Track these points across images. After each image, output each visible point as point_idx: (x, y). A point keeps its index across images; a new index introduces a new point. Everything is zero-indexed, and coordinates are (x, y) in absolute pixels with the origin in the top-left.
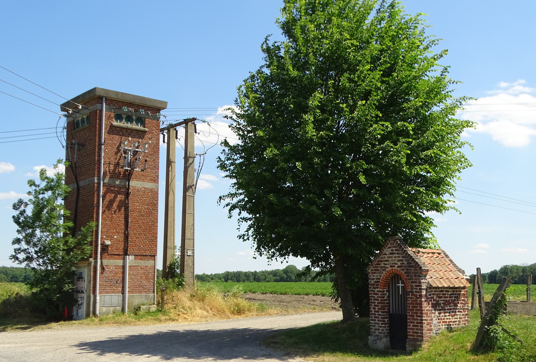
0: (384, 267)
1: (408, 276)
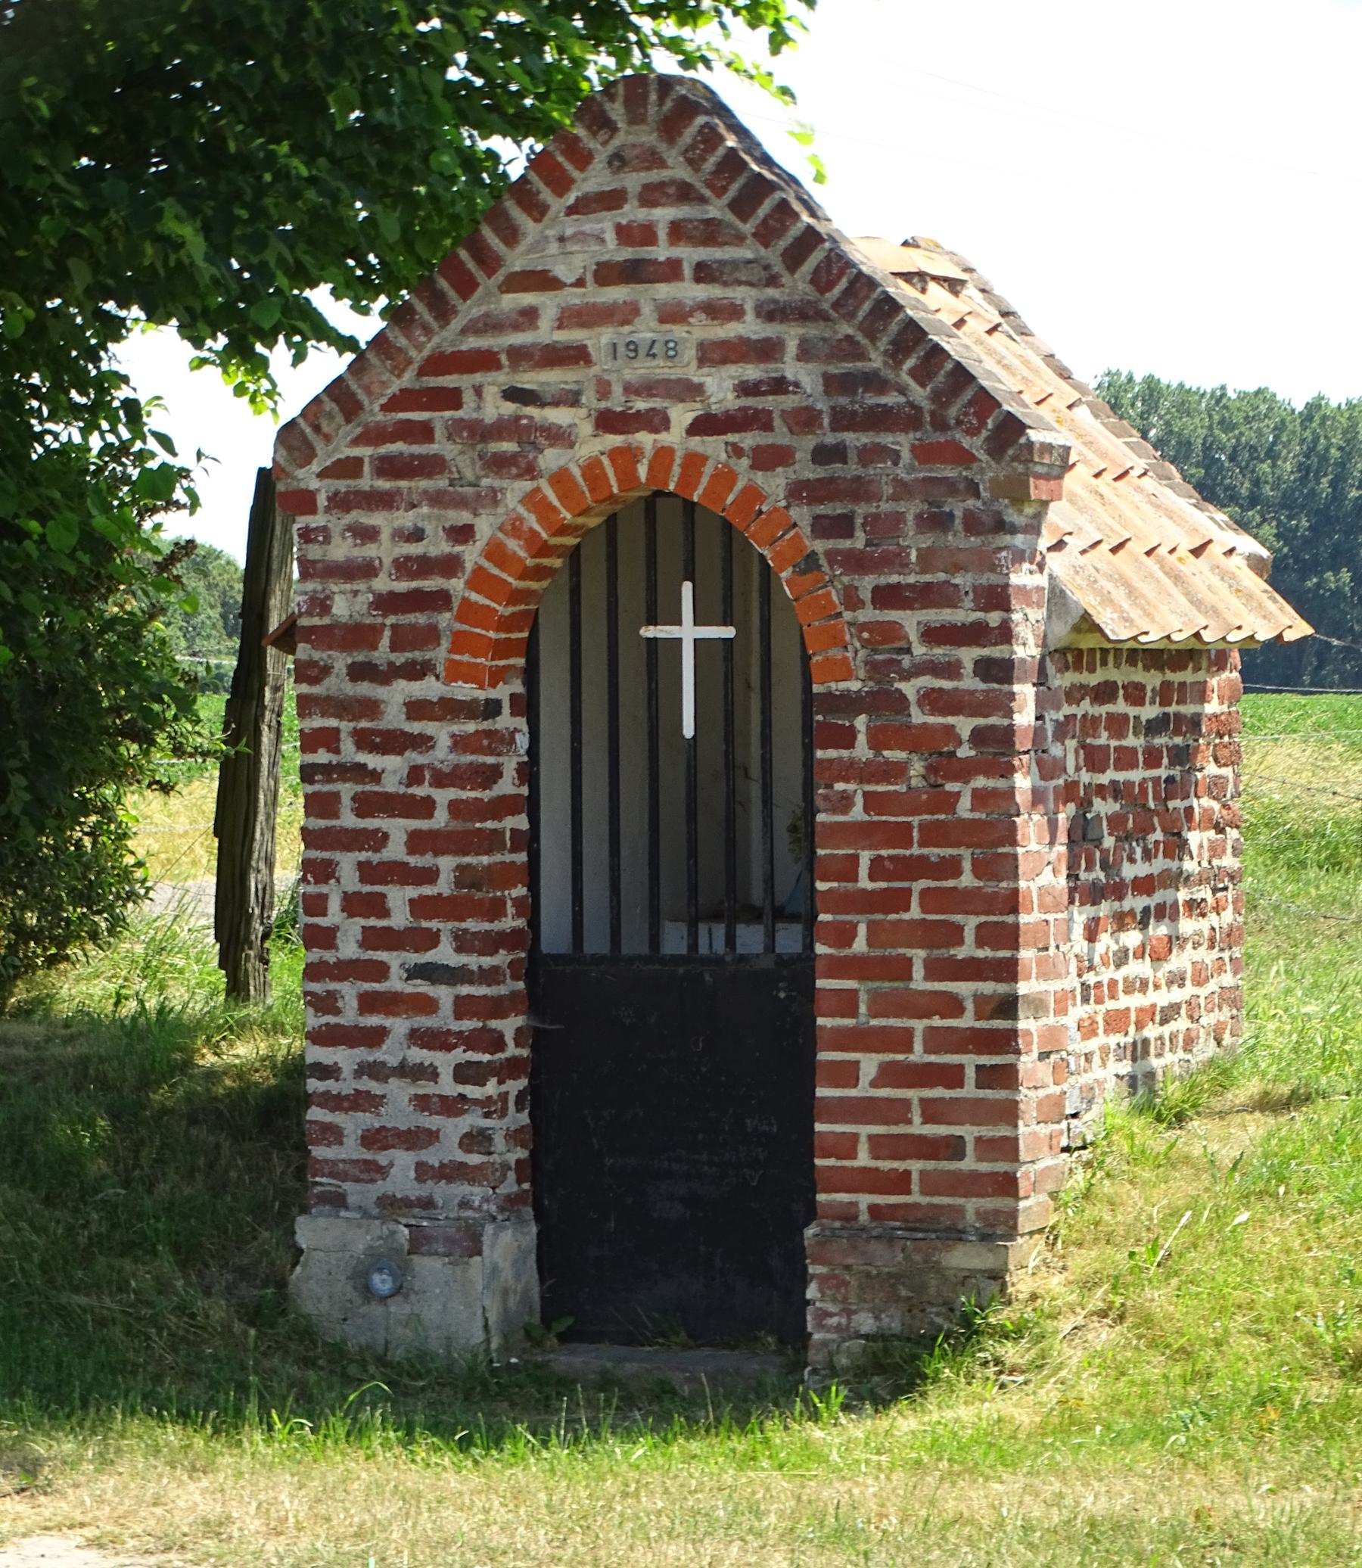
0: (502, 429)
1: (824, 527)
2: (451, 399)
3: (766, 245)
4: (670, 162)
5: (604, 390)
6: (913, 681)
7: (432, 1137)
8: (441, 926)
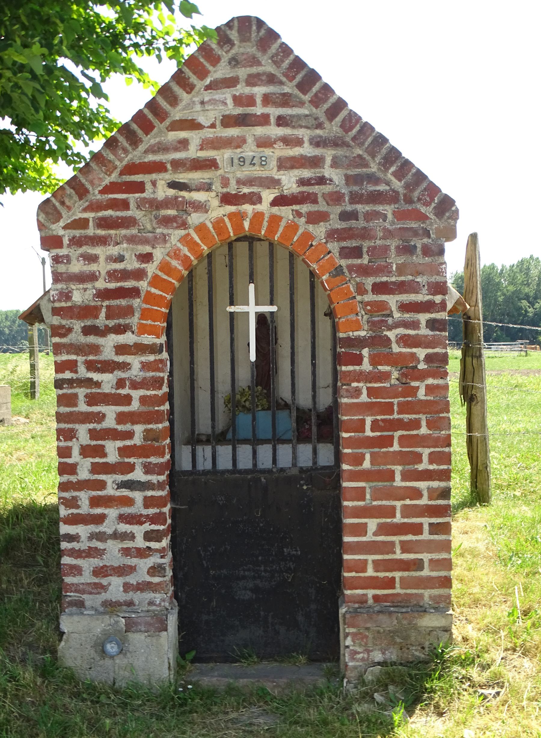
0: (167, 203)
1: (346, 253)
2: (140, 187)
3: (317, 107)
4: (263, 62)
5: (225, 182)
6: (394, 331)
7: (132, 569)
8: (136, 461)
